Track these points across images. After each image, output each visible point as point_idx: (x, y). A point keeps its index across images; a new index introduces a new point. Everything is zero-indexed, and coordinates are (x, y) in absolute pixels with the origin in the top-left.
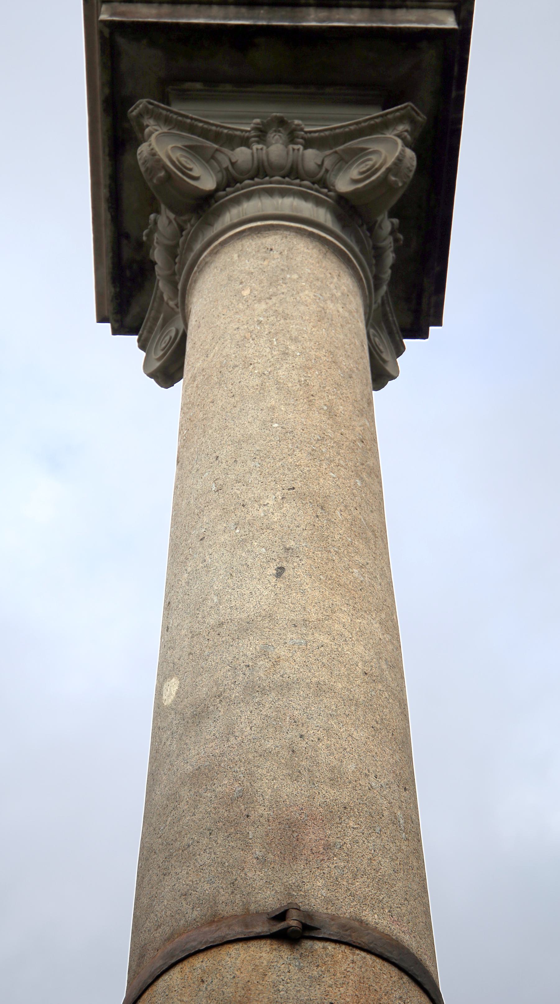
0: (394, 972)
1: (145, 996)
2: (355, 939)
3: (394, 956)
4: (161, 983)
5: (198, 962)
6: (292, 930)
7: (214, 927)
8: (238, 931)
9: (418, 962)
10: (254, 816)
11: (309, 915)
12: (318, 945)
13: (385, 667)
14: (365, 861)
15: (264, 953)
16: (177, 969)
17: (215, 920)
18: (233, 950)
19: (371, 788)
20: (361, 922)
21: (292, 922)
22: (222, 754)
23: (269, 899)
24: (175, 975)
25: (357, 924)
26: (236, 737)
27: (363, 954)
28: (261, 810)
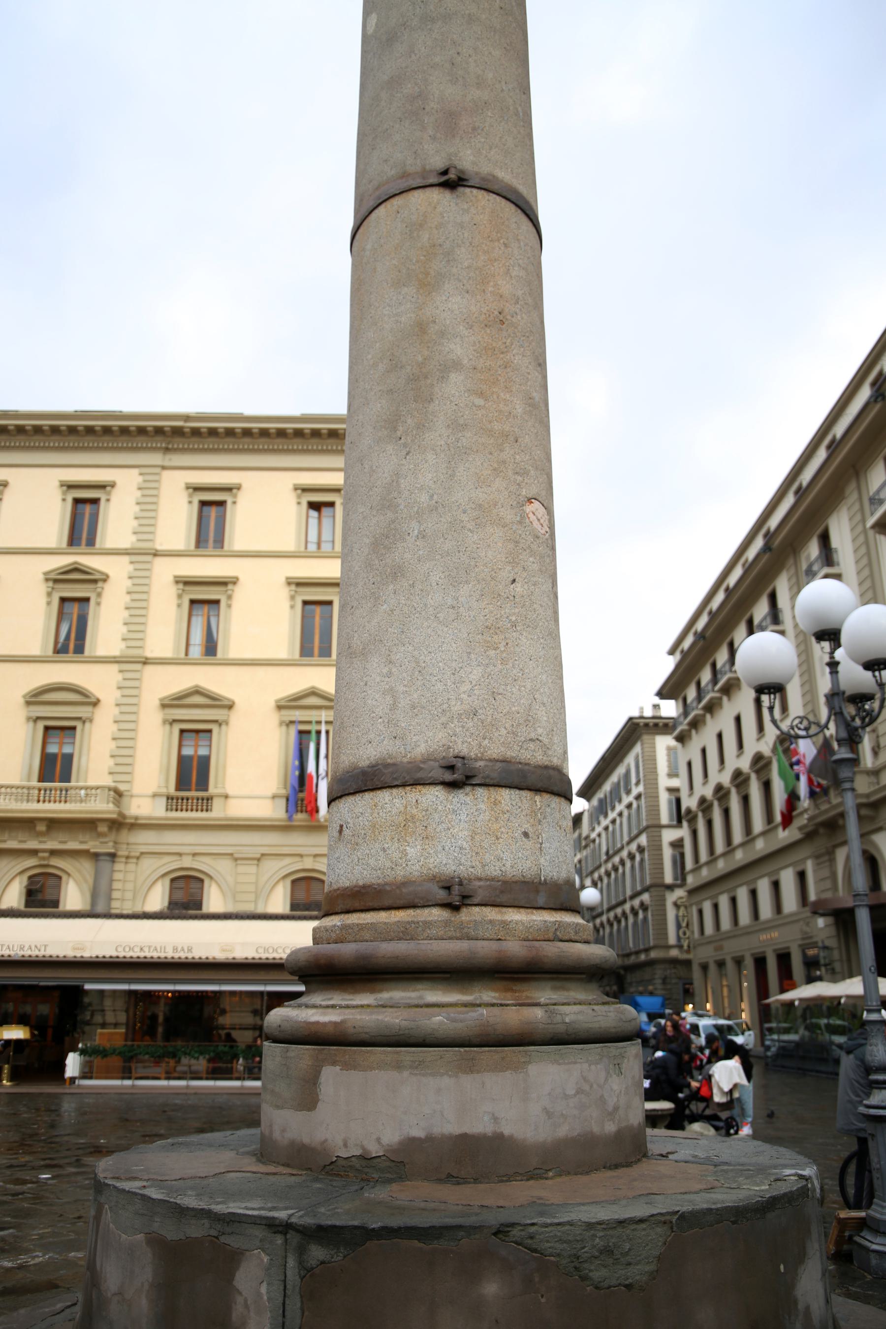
0: (513, 207)
1: (365, 223)
2: (489, 187)
3: (513, 198)
4: (373, 215)
5: (396, 201)
6: (452, 181)
7: (404, 180)
8: (419, 182)
9: (527, 203)
10: (428, 108)
11: (462, 172)
12: (468, 190)
13: (514, 4)
14: (497, 139)
15: (436, 195)
16: (383, 206)
17: (404, 175)
18: (416, 193)
19: (502, 91)
20: (494, 176)
21: (452, 176)
22: (407, 67)
23: (439, 163)
24: (381, 210)
25: (491, 178)
26: (416, 55)
27: (495, 196)
28: (432, 105)
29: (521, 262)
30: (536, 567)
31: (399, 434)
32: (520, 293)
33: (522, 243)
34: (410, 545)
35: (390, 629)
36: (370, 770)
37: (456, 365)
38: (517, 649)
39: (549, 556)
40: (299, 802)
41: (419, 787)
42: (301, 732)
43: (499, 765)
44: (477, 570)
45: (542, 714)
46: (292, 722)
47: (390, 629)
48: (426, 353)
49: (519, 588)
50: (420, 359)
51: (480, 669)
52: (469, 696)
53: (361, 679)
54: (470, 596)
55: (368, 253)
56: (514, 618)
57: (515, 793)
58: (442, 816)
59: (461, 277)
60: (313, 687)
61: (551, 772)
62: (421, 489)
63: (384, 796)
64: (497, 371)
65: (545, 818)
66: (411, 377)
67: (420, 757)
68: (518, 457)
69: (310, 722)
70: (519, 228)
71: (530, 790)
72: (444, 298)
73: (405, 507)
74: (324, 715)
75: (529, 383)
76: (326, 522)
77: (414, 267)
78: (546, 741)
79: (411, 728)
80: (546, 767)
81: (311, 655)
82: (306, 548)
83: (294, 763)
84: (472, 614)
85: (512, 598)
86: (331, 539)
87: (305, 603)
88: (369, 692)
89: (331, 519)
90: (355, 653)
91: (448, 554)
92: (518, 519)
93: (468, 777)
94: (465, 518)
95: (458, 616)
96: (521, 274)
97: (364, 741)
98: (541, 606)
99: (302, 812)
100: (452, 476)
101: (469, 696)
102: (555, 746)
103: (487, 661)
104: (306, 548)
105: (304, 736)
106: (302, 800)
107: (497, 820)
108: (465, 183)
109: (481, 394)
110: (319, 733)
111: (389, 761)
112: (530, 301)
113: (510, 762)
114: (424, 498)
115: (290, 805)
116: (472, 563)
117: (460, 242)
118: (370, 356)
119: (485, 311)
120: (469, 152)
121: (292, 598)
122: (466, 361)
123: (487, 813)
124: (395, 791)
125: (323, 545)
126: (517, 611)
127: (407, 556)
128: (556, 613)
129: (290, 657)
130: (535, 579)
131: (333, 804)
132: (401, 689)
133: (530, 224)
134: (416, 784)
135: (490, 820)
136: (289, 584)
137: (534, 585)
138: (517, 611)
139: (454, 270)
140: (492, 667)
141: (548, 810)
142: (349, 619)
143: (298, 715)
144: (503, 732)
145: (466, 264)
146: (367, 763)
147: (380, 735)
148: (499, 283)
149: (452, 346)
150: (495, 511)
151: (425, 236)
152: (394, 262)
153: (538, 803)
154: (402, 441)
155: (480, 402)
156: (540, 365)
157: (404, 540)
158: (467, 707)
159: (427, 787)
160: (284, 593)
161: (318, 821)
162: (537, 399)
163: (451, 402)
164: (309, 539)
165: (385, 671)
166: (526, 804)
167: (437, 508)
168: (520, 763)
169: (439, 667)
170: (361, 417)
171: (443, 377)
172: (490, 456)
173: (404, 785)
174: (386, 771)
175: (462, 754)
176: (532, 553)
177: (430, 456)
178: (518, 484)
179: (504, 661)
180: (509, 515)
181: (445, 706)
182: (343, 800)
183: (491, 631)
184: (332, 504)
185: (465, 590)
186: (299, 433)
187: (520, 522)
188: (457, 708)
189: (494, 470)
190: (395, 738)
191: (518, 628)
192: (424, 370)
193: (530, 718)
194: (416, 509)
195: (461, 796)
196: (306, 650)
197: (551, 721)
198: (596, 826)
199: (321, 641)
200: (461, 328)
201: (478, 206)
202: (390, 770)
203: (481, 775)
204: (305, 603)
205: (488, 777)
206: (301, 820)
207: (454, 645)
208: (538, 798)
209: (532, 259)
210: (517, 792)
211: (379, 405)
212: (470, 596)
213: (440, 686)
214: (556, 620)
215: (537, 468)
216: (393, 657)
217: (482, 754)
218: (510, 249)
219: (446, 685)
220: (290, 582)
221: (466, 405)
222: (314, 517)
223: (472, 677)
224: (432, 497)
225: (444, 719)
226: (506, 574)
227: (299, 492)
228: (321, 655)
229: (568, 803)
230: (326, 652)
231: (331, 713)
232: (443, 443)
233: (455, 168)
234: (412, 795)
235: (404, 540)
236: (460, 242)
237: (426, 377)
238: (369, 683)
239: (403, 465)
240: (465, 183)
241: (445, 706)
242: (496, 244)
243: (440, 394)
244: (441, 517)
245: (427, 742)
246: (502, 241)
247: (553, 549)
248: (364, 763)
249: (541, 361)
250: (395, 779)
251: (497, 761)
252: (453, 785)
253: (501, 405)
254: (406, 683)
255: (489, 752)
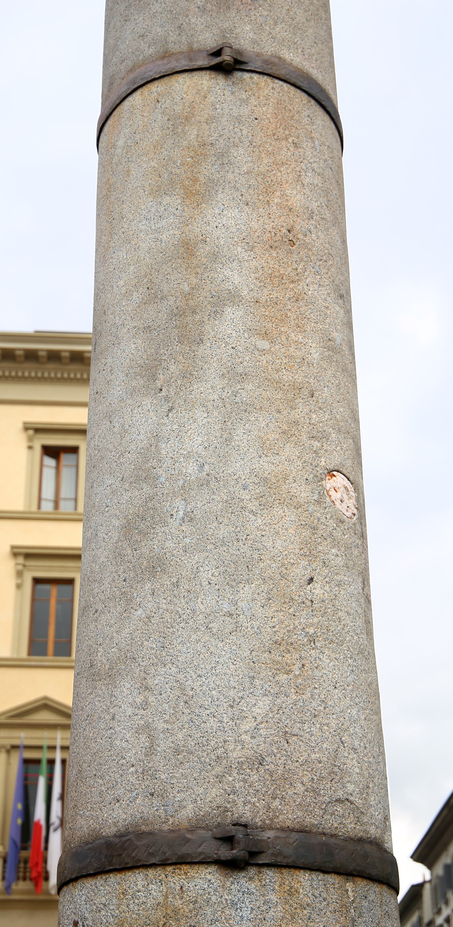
0: (304, 96)
1: (115, 113)
2: (274, 71)
3: (304, 85)
4: (126, 103)
5: (154, 87)
6: (226, 64)
7: (165, 61)
8: (184, 64)
9: (323, 91)
11: (239, 52)
12: (247, 75)
14: (284, 11)
15: (206, 81)
16: (139, 92)
17: (166, 55)
18: (181, 78)
20: (280, 58)
21: (226, 57)
23: (209, 40)
24: (137, 95)
25: (276, 60)
27: (281, 83)
29: (315, 165)
30: (340, 561)
31: (159, 384)
32: (314, 205)
33: (317, 143)
34: (173, 530)
35: (146, 643)
36: (117, 840)
37: (233, 297)
38: (317, 673)
39: (357, 546)
40: (22, 865)
41: (184, 867)
42: (26, 762)
43: (294, 836)
44: (262, 565)
45: (352, 763)
46: (14, 747)
47: (146, 643)
48: (194, 281)
49: (317, 590)
50: (187, 288)
51: (267, 700)
52: (253, 737)
53: (107, 711)
54: (253, 600)
55: (119, 151)
56: (312, 631)
57: (318, 878)
58: (216, 911)
59: (238, 185)
60: (46, 698)
61: (368, 847)
62: (188, 457)
63: (137, 880)
64: (285, 305)
65: (360, 916)
66: (176, 311)
67: (185, 824)
68: (314, 416)
69: (39, 748)
70: (313, 123)
71: (338, 873)
72: (217, 211)
73: (167, 479)
74: (59, 738)
75: (328, 321)
76: (67, 473)
77: (178, 171)
78: (359, 802)
79: (174, 781)
80: (360, 840)
81: (44, 653)
82: (39, 507)
83: (15, 806)
84: (256, 624)
85: (309, 603)
86: (73, 496)
87: (37, 581)
88: (118, 729)
89: (74, 470)
90: (99, 674)
91: (223, 544)
92: (315, 498)
93: (253, 854)
94: (245, 495)
95: (238, 627)
96: (316, 182)
97: (109, 798)
98: (348, 614)
99: (24, 879)
100: (228, 441)
101: (253, 737)
102: (372, 810)
103: (276, 689)
104: (39, 507)
105: (32, 768)
106: (26, 862)
107: (293, 917)
108: (243, 67)
109: (265, 335)
110: (51, 762)
111: (143, 828)
112: (328, 215)
113: (309, 832)
114: (191, 468)
115: (8, 870)
116: (256, 556)
117: (237, 140)
118: (122, 283)
119: (269, 229)
120: (247, 28)
121: (19, 574)
122: (245, 293)
123: (279, 908)
124: (151, 873)
125: (62, 504)
126: (316, 620)
127: (169, 544)
128: (368, 622)
129: (15, 656)
130: (338, 578)
131: (65, 889)
132: (161, 725)
133: (327, 118)
134: (181, 863)
135: (283, 918)
136: (15, 555)
137: (339, 585)
138: (316, 620)
139: (230, 176)
140: (283, 698)
141: (365, 904)
142: (92, 626)
143: (23, 737)
144: (300, 788)
145: (245, 168)
146: (114, 830)
147: (131, 791)
148: (288, 192)
149: (228, 273)
150: (284, 487)
151: (192, 133)
152: (153, 164)
153: (350, 893)
154: (163, 393)
155: (264, 344)
156: (341, 296)
157: (165, 524)
158: (250, 753)
159: (196, 867)
160: (20, 440)
161: (48, 893)
162: (338, 341)
163: (227, 344)
164: (44, 496)
165: (139, 700)
166: (334, 896)
167: (208, 482)
168: (324, 834)
169: (212, 697)
170: (110, 360)
171: (216, 312)
172: (278, 415)
173: (164, 864)
174: (139, 843)
175: (243, 820)
176: (335, 543)
177: (200, 414)
178: (315, 452)
179: (299, 690)
180: (304, 493)
181: (220, 751)
182: (79, 885)
183: (282, 648)
184: (74, 450)
185: (246, 592)
186: (31, 356)
187: (318, 502)
188: (236, 754)
189: (284, 433)
190: (152, 795)
191: (318, 644)
192: (191, 303)
193: (336, 769)
194: (181, 483)
195: (243, 881)
196: (37, 646)
197: (366, 773)
198: (443, 907)
199: (57, 635)
200: (239, 249)
201: (262, 95)
202: (144, 841)
203: (270, 851)
204: (37, 581)
205: (280, 853)
206: (23, 892)
207: (232, 666)
208: (349, 886)
209: (330, 162)
210: (321, 876)
211: (133, 346)
212: (253, 600)
213: (212, 723)
214: (369, 633)
215: (339, 431)
216: (150, 682)
217: (271, 820)
218: (301, 150)
219: (221, 722)
220: (27, 427)
221: (247, 348)
222: (48, 466)
223: (257, 710)
224: (202, 466)
225: (218, 770)
226: (300, 571)
227: (31, 432)
228: (57, 653)
229: (393, 892)
230: (63, 648)
231: (67, 734)
232: (216, 397)
233: (231, 48)
234: (175, 879)
235: (165, 524)
236: (237, 140)
237: (194, 312)
238: (117, 717)
239: (163, 424)
240: (243, 67)
241: (220, 751)
242: (284, 143)
243: (213, 333)
244: (214, 493)
245: (195, 801)
246: (290, 140)
247: (363, 536)
248: (109, 831)
249: (343, 292)
250: (152, 855)
251: (292, 830)
252: (232, 866)
253: (292, 349)
254: (167, 717)
255: (281, 817)
